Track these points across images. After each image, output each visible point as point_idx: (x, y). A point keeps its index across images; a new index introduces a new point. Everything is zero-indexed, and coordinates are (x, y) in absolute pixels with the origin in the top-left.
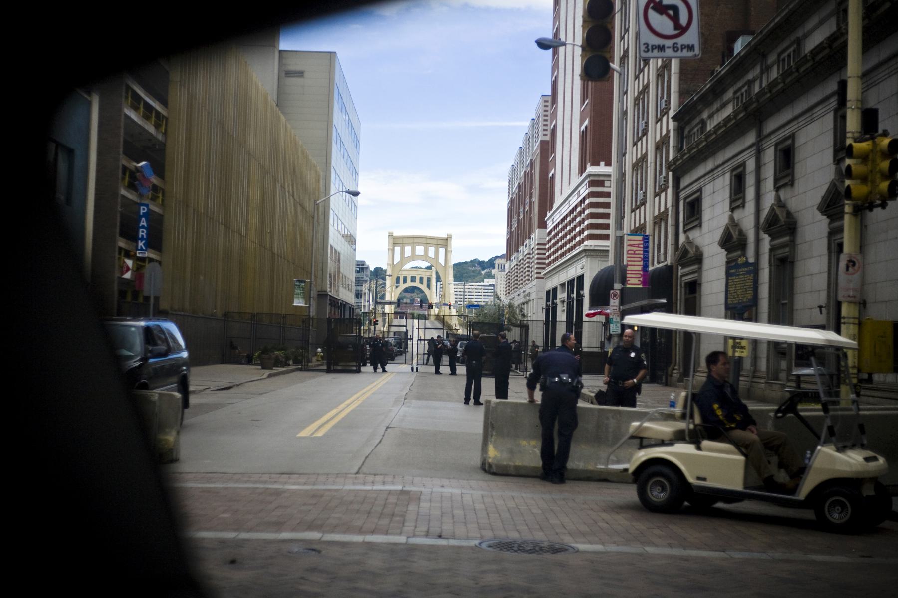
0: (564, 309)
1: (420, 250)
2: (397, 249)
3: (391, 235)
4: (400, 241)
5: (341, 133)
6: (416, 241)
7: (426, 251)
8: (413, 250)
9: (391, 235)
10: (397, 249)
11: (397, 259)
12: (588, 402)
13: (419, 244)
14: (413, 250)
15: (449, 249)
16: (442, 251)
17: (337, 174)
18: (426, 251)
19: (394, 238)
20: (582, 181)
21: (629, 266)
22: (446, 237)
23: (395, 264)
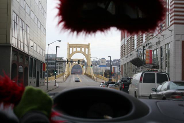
0: (166, 61)
1: (79, 49)
2: (71, 49)
3: (68, 44)
4: (72, 46)
5: (41, 20)
6: (77, 46)
7: (81, 49)
8: (76, 49)
9: (68, 44)
10: (71, 49)
11: (71, 52)
12: (31, 59)
13: (79, 47)
14: (76, 49)
15: (89, 48)
16: (87, 49)
17: (35, 15)
18: (81, 49)
19: (70, 45)
20: (177, 19)
21: (111, 60)
22: (88, 44)
23: (70, 54)
